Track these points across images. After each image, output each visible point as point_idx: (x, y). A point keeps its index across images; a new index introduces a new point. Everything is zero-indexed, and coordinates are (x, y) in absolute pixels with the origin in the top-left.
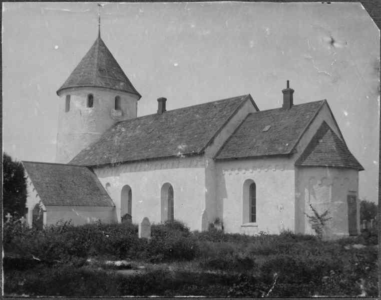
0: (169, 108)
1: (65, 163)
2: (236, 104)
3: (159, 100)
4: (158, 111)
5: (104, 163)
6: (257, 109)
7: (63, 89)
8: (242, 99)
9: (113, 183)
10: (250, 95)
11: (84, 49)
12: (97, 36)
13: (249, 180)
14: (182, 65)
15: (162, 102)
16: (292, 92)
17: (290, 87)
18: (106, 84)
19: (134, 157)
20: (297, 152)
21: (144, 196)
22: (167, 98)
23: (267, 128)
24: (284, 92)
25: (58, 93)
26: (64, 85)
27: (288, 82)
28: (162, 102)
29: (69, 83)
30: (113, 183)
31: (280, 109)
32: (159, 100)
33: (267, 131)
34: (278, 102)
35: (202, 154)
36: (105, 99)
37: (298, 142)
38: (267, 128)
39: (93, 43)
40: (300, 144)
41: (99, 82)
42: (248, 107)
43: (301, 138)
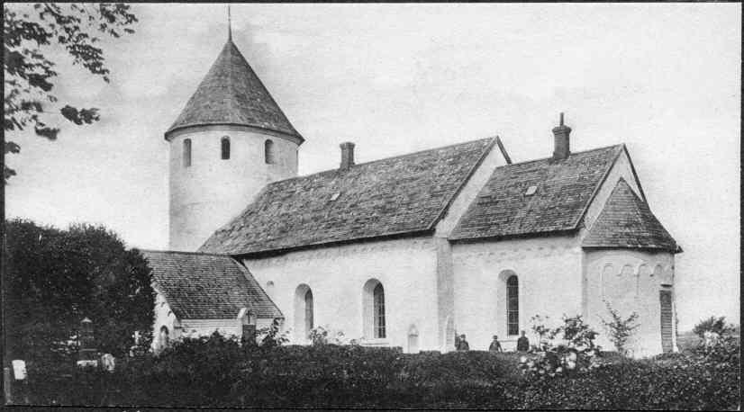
0: (359, 158)
1: (194, 251)
2: (469, 156)
3: (342, 147)
4: (342, 165)
5: (302, 245)
6: (509, 161)
7: (174, 131)
8: (486, 144)
9: (278, 280)
10: (498, 137)
11: (210, 57)
12: (227, 38)
13: (371, 281)
14: (368, 94)
15: (349, 148)
16: (568, 131)
17: (565, 124)
18: (249, 119)
19: (415, 223)
20: (585, 227)
21: (321, 303)
22: (338, 145)
23: (531, 190)
24: (556, 132)
25: (168, 136)
26: (175, 124)
27: (562, 115)
28: (349, 148)
29: (188, 120)
30: (278, 280)
31: (550, 161)
32: (342, 147)
33: (532, 195)
34: (547, 148)
35: (429, 233)
36: (247, 146)
37: (586, 211)
38: (531, 190)
39: (221, 49)
40: (588, 215)
41: (236, 116)
42: (496, 160)
43: (589, 206)
